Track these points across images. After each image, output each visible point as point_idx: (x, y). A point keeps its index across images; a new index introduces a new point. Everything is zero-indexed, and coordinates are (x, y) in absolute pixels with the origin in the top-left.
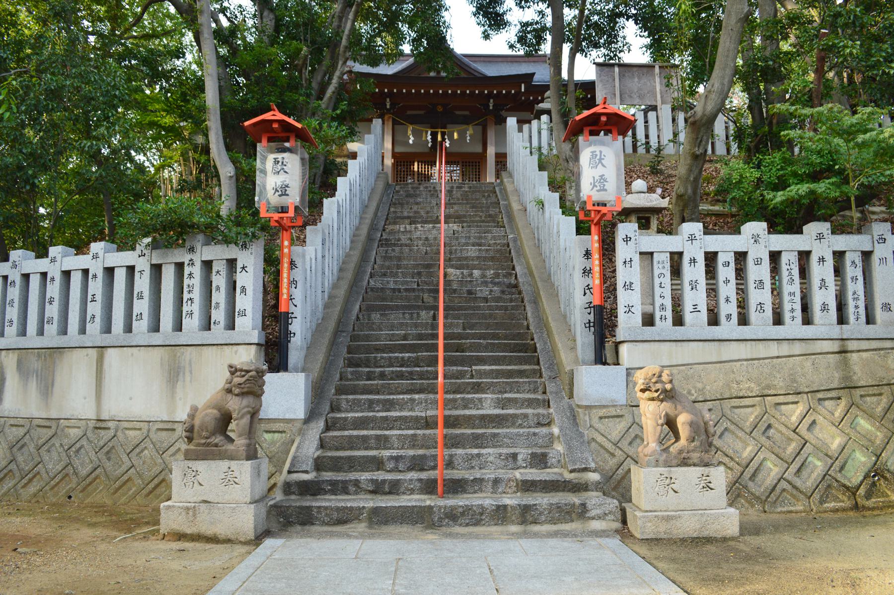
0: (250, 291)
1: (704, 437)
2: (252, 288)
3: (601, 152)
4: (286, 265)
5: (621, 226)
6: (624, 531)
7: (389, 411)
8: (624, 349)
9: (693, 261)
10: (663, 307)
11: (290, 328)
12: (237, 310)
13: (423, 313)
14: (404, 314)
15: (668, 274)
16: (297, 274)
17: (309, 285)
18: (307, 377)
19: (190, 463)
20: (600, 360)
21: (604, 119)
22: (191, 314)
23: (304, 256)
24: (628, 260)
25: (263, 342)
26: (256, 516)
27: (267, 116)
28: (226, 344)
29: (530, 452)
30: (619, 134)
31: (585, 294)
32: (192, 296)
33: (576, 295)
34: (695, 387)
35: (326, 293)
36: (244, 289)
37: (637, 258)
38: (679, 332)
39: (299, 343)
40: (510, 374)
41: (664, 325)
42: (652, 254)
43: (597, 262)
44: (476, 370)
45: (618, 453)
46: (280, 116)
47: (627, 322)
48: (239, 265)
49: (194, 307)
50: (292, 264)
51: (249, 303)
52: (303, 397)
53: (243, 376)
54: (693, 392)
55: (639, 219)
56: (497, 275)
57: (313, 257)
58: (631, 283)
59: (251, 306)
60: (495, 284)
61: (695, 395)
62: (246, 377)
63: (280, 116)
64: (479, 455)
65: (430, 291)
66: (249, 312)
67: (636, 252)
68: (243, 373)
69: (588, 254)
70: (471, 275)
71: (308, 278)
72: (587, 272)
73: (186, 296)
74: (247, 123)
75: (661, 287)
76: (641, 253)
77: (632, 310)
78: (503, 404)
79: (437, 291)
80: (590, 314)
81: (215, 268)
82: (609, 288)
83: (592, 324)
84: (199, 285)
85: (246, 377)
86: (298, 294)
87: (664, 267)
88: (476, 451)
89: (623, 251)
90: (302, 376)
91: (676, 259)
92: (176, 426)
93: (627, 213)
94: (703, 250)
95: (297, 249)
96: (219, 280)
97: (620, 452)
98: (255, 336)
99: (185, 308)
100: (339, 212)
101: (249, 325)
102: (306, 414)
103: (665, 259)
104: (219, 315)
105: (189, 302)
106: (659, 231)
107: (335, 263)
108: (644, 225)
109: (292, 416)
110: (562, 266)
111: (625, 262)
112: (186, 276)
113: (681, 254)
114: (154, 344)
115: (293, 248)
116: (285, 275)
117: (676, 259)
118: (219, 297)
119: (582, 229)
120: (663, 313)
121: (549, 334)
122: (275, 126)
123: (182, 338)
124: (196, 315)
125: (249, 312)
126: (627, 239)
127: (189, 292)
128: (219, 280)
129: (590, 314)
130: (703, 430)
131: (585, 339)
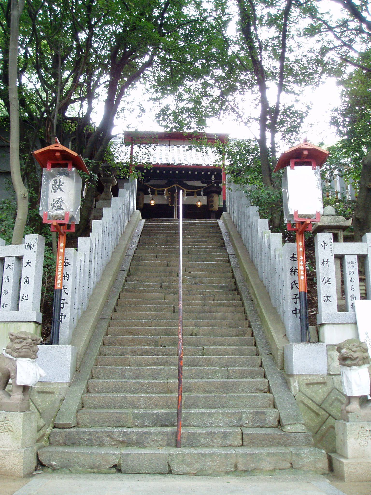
0: (32, 281)
4: (61, 262)
6: (332, 470)
11: (62, 311)
12: (21, 296)
15: (357, 272)
16: (69, 270)
17: (78, 280)
20: (304, 338)
21: (306, 153)
24: (326, 260)
25: (40, 321)
27: (52, 147)
29: (252, 411)
30: (317, 165)
31: (292, 288)
35: (91, 290)
36: (27, 279)
39: (68, 323)
43: (302, 263)
45: (322, 412)
46: (61, 147)
48: (25, 261)
50: (66, 262)
51: (32, 291)
53: (21, 342)
58: (328, 279)
59: (33, 292)
63: (61, 147)
64: (210, 414)
66: (30, 297)
67: (331, 255)
69: (294, 258)
70: (201, 282)
71: (78, 275)
72: (294, 271)
74: (36, 152)
77: (330, 299)
82: (311, 279)
83: (298, 311)
85: (23, 344)
87: (353, 266)
88: (208, 411)
90: (69, 348)
95: (71, 251)
100: (103, 231)
111: (323, 262)
121: (263, 321)
122: (58, 154)
125: (30, 297)
129: (296, 303)
131: (292, 322)
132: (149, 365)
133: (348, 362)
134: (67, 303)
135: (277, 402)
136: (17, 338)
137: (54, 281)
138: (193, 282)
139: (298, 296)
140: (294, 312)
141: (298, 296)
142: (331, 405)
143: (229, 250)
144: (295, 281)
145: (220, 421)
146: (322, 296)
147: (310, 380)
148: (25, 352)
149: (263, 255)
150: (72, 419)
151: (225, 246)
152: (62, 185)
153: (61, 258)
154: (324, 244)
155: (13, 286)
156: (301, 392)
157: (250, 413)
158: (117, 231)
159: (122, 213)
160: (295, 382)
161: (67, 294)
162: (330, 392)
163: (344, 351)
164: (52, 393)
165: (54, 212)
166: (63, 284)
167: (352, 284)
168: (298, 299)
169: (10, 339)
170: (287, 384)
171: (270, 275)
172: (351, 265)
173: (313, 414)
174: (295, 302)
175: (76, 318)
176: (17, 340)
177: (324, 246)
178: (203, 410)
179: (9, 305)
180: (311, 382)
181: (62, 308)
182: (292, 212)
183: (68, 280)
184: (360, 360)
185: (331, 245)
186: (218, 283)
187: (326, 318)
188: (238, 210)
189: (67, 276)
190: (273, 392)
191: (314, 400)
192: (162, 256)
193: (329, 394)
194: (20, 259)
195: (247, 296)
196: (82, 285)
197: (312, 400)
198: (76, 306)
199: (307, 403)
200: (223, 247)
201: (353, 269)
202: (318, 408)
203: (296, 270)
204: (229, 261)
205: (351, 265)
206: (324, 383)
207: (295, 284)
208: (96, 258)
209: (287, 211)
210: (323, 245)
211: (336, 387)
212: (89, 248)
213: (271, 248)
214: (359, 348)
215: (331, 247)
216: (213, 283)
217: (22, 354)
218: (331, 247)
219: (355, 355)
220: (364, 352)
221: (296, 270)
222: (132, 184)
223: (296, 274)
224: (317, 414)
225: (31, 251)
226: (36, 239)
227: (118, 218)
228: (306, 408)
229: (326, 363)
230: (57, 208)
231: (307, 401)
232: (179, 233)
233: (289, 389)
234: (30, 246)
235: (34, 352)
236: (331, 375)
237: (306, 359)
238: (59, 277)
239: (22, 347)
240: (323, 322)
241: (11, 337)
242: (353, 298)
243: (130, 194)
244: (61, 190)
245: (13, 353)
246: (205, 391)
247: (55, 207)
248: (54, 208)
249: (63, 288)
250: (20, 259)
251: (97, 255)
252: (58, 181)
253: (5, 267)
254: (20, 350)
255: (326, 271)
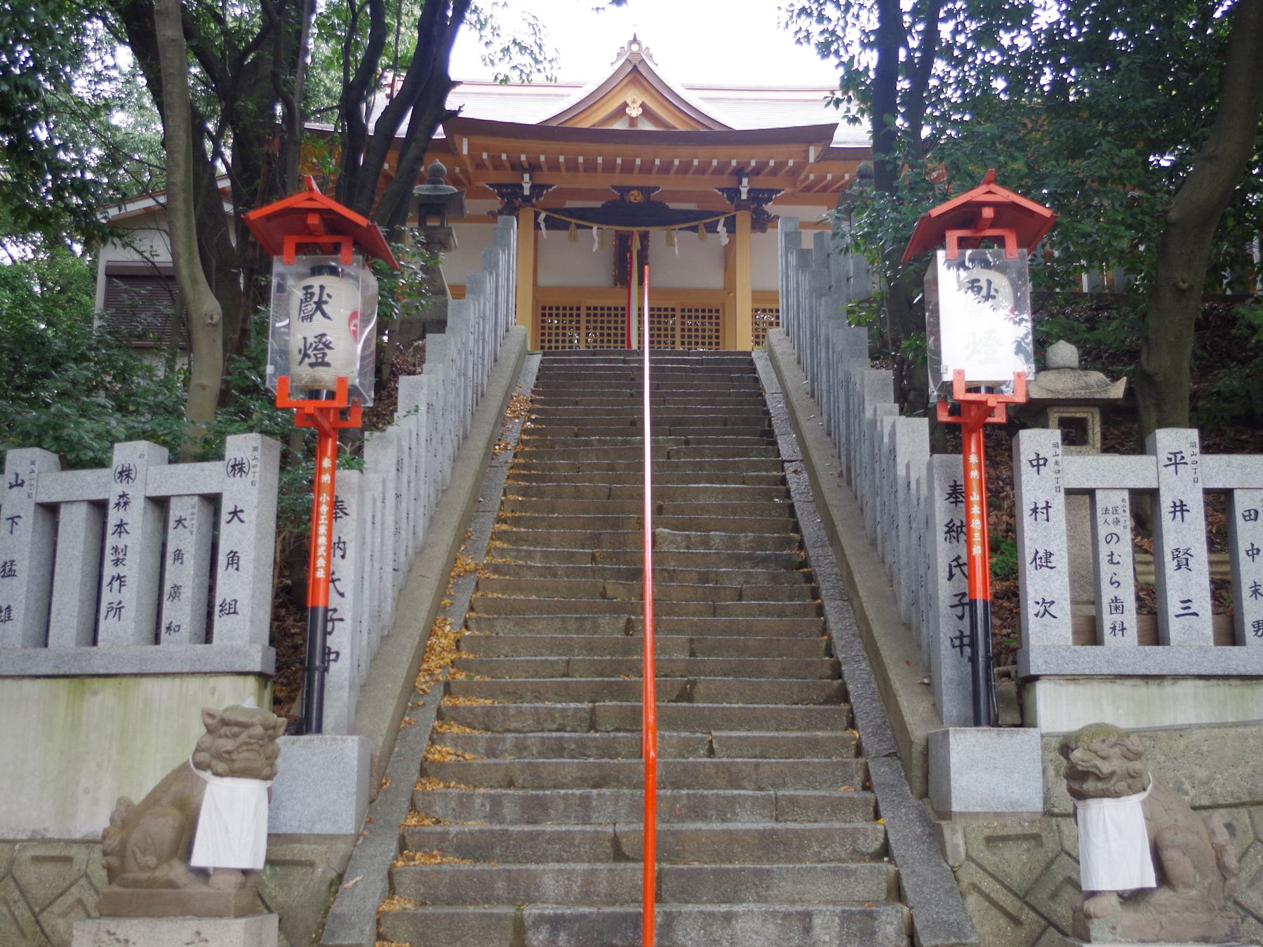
0: (246, 561)
1: (1214, 878)
2: (252, 556)
3: (989, 282)
4: (324, 509)
5: (1024, 434)
7: (536, 822)
8: (1043, 692)
9: (1180, 508)
10: (1117, 606)
12: (218, 601)
13: (605, 620)
14: (563, 620)
15: (1127, 537)
16: (347, 528)
17: (368, 553)
18: (362, 744)
19: (111, 924)
22: (118, 609)
23: (361, 491)
24: (1041, 505)
25: (271, 670)
26: (1028, 662)
28: (193, 674)
31: (951, 576)
32: (121, 570)
33: (943, 570)
34: (1191, 777)
37: (1059, 501)
38: (1154, 659)
39: (347, 675)
40: (794, 749)
41: (1123, 643)
42: (1091, 493)
44: (719, 739)
45: (1027, 916)
47: (1048, 635)
48: (227, 507)
49: (129, 595)
50: (337, 508)
51: (248, 587)
52: (353, 788)
53: (235, 736)
54: (1187, 786)
55: (1064, 423)
56: (760, 544)
57: (378, 494)
60: (757, 562)
61: (1192, 792)
62: (243, 737)
65: (618, 574)
66: (244, 606)
67: (1058, 489)
68: (236, 729)
70: (706, 543)
72: (957, 530)
73: (109, 571)
75: (1111, 562)
76: (1070, 492)
77: (1052, 609)
78: (778, 809)
79: (639, 573)
80: (961, 618)
81: (175, 512)
83: (966, 641)
84: (138, 548)
85: (243, 737)
86: (346, 569)
87: (1117, 522)
88: (724, 908)
89: (1034, 488)
91: (1144, 507)
92: (73, 851)
93: (1031, 413)
94: (1200, 486)
95: (349, 476)
96: (186, 540)
97: (1032, 914)
98: (257, 656)
99: (107, 597)
101: (246, 631)
102: (358, 822)
103: (1119, 504)
104: (181, 612)
105: (116, 584)
106: (1106, 449)
107: (421, 511)
108: (1074, 435)
109: (328, 829)
110: (902, 520)
111: (1035, 510)
112: (110, 528)
113: (1154, 493)
114: (34, 671)
115: (342, 474)
116: (323, 530)
117: (1144, 507)
118: (184, 576)
119: (947, 439)
120: (1118, 618)
122: (313, 220)
123: (98, 660)
124: (130, 612)
126: (1039, 463)
127: (117, 562)
128: (186, 540)
129: (961, 618)
130: (1213, 863)
132: (563, 786)
133: (1090, 785)
134: (341, 620)
135: (907, 885)
136: (225, 723)
137: (278, 526)
138: (683, 544)
139: (966, 600)
140: (957, 642)
141: (966, 600)
142: (1054, 896)
143: (787, 446)
144: (959, 557)
145: (755, 937)
146: (1030, 602)
147: (995, 827)
148: (247, 759)
149: (877, 475)
150: (367, 932)
151: (770, 433)
152: (326, 302)
153: (325, 498)
154: (1038, 459)
155: (196, 575)
156: (973, 860)
157: (833, 913)
158: (465, 396)
159: (477, 341)
160: (954, 832)
161: (342, 595)
162: (1052, 862)
163: (1076, 755)
164: (312, 864)
165: (304, 373)
166: (332, 568)
167: (1114, 568)
168: (967, 608)
169: (206, 726)
170: (935, 837)
171: (894, 532)
172: (1110, 518)
173: (1003, 921)
174: (960, 613)
175: (364, 658)
176: (225, 730)
177: (1038, 465)
178: (709, 908)
179: (186, 629)
180: (1000, 833)
181: (330, 633)
182: (947, 377)
183: (343, 557)
184: (1118, 781)
185: (1057, 463)
186: (752, 548)
187: (1040, 662)
188: (811, 332)
189: (341, 546)
190: (897, 860)
191: (1008, 881)
192: (593, 467)
193: (1047, 868)
194: (213, 501)
195: (834, 588)
196: (377, 565)
197: (1001, 883)
198: (365, 626)
199: (987, 891)
200: (768, 436)
201: (1117, 529)
202: (1018, 903)
203: (962, 526)
204: (783, 481)
205: (1110, 518)
206: (1036, 837)
207: (959, 565)
208: (412, 485)
209: (938, 373)
210: (1035, 463)
211: (1066, 848)
212: (394, 461)
213: (898, 460)
214: (1116, 750)
215: (1057, 468)
216: (737, 546)
217: (237, 765)
218: (1057, 468)
219: (1106, 768)
220: (1130, 760)
221: (962, 526)
222: (503, 251)
223: (963, 537)
224: (1016, 921)
225: (239, 482)
226: (255, 449)
227: (466, 358)
228: (987, 904)
229: (1039, 784)
230: (313, 360)
231: (987, 884)
232: (642, 394)
233: (942, 851)
234: (238, 468)
235: (267, 759)
236: (1052, 815)
237: (990, 772)
238: (322, 551)
239: (240, 746)
240: (1032, 672)
241: (210, 721)
242: (1117, 608)
243: (497, 282)
244: (324, 314)
245: (214, 762)
246: (716, 856)
247: (309, 356)
248: (307, 360)
249: (331, 579)
250: (213, 501)
251: (413, 475)
252: (316, 290)
253: (172, 524)
254: (235, 756)
255: (1044, 536)
